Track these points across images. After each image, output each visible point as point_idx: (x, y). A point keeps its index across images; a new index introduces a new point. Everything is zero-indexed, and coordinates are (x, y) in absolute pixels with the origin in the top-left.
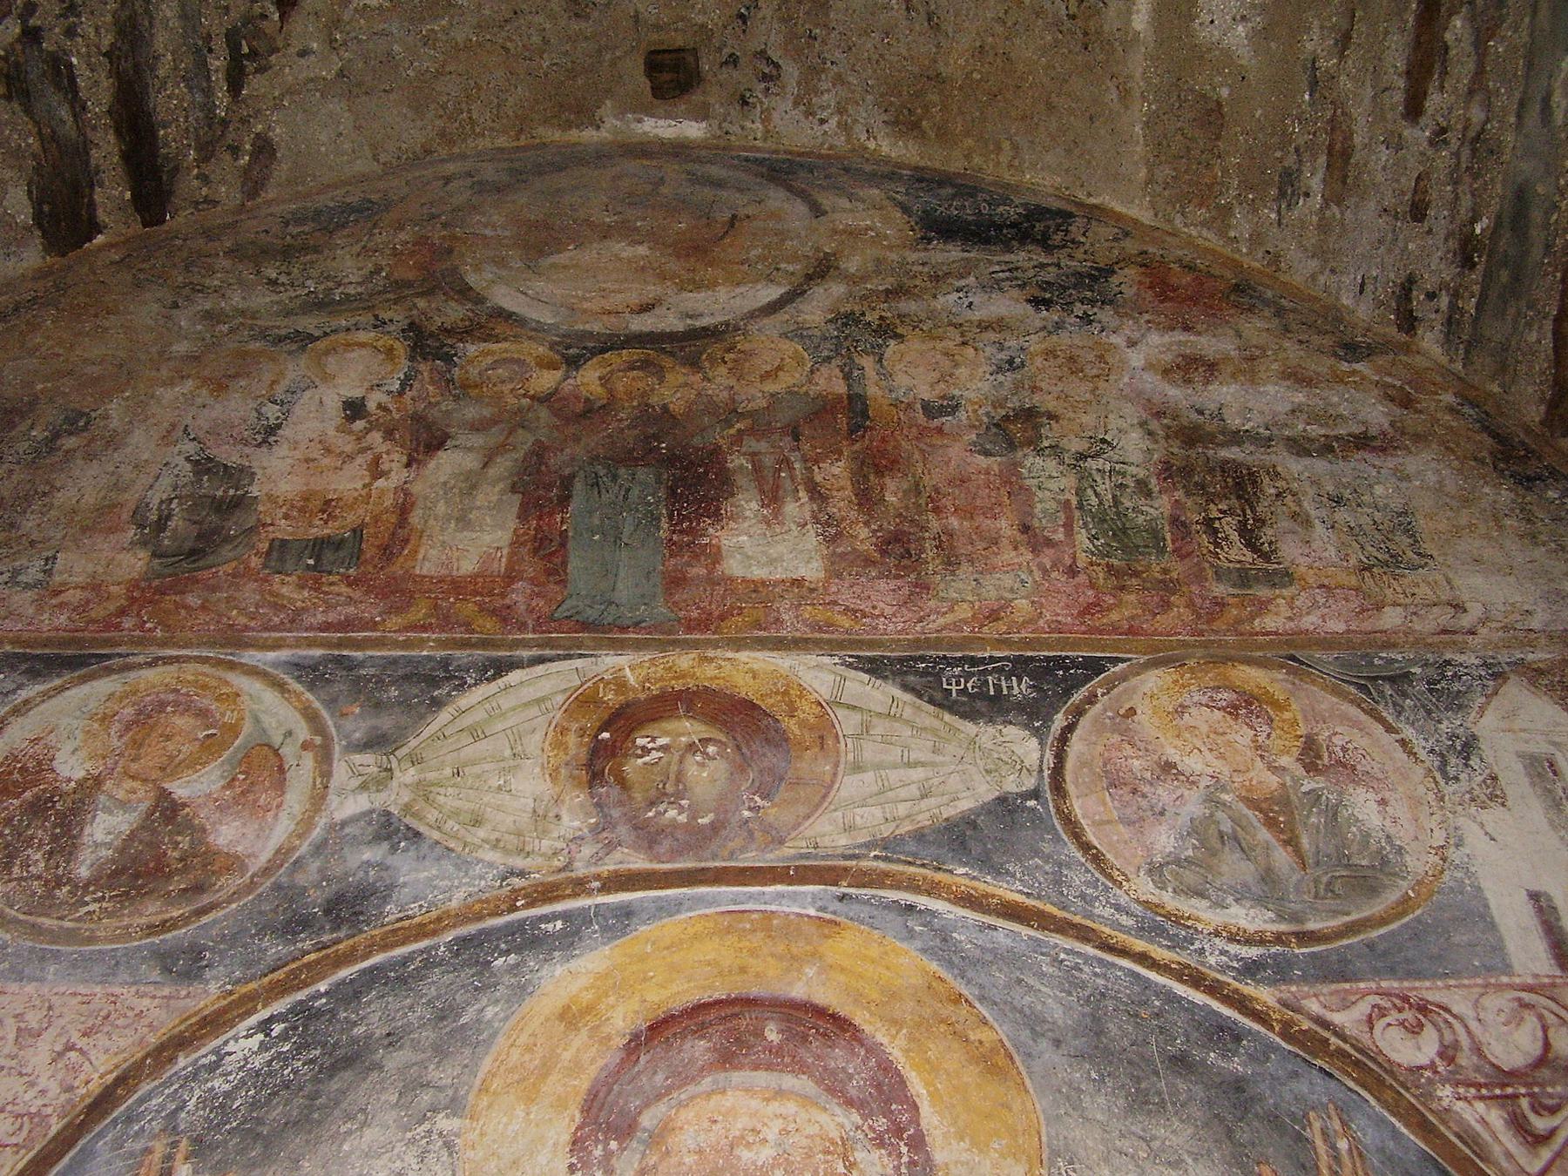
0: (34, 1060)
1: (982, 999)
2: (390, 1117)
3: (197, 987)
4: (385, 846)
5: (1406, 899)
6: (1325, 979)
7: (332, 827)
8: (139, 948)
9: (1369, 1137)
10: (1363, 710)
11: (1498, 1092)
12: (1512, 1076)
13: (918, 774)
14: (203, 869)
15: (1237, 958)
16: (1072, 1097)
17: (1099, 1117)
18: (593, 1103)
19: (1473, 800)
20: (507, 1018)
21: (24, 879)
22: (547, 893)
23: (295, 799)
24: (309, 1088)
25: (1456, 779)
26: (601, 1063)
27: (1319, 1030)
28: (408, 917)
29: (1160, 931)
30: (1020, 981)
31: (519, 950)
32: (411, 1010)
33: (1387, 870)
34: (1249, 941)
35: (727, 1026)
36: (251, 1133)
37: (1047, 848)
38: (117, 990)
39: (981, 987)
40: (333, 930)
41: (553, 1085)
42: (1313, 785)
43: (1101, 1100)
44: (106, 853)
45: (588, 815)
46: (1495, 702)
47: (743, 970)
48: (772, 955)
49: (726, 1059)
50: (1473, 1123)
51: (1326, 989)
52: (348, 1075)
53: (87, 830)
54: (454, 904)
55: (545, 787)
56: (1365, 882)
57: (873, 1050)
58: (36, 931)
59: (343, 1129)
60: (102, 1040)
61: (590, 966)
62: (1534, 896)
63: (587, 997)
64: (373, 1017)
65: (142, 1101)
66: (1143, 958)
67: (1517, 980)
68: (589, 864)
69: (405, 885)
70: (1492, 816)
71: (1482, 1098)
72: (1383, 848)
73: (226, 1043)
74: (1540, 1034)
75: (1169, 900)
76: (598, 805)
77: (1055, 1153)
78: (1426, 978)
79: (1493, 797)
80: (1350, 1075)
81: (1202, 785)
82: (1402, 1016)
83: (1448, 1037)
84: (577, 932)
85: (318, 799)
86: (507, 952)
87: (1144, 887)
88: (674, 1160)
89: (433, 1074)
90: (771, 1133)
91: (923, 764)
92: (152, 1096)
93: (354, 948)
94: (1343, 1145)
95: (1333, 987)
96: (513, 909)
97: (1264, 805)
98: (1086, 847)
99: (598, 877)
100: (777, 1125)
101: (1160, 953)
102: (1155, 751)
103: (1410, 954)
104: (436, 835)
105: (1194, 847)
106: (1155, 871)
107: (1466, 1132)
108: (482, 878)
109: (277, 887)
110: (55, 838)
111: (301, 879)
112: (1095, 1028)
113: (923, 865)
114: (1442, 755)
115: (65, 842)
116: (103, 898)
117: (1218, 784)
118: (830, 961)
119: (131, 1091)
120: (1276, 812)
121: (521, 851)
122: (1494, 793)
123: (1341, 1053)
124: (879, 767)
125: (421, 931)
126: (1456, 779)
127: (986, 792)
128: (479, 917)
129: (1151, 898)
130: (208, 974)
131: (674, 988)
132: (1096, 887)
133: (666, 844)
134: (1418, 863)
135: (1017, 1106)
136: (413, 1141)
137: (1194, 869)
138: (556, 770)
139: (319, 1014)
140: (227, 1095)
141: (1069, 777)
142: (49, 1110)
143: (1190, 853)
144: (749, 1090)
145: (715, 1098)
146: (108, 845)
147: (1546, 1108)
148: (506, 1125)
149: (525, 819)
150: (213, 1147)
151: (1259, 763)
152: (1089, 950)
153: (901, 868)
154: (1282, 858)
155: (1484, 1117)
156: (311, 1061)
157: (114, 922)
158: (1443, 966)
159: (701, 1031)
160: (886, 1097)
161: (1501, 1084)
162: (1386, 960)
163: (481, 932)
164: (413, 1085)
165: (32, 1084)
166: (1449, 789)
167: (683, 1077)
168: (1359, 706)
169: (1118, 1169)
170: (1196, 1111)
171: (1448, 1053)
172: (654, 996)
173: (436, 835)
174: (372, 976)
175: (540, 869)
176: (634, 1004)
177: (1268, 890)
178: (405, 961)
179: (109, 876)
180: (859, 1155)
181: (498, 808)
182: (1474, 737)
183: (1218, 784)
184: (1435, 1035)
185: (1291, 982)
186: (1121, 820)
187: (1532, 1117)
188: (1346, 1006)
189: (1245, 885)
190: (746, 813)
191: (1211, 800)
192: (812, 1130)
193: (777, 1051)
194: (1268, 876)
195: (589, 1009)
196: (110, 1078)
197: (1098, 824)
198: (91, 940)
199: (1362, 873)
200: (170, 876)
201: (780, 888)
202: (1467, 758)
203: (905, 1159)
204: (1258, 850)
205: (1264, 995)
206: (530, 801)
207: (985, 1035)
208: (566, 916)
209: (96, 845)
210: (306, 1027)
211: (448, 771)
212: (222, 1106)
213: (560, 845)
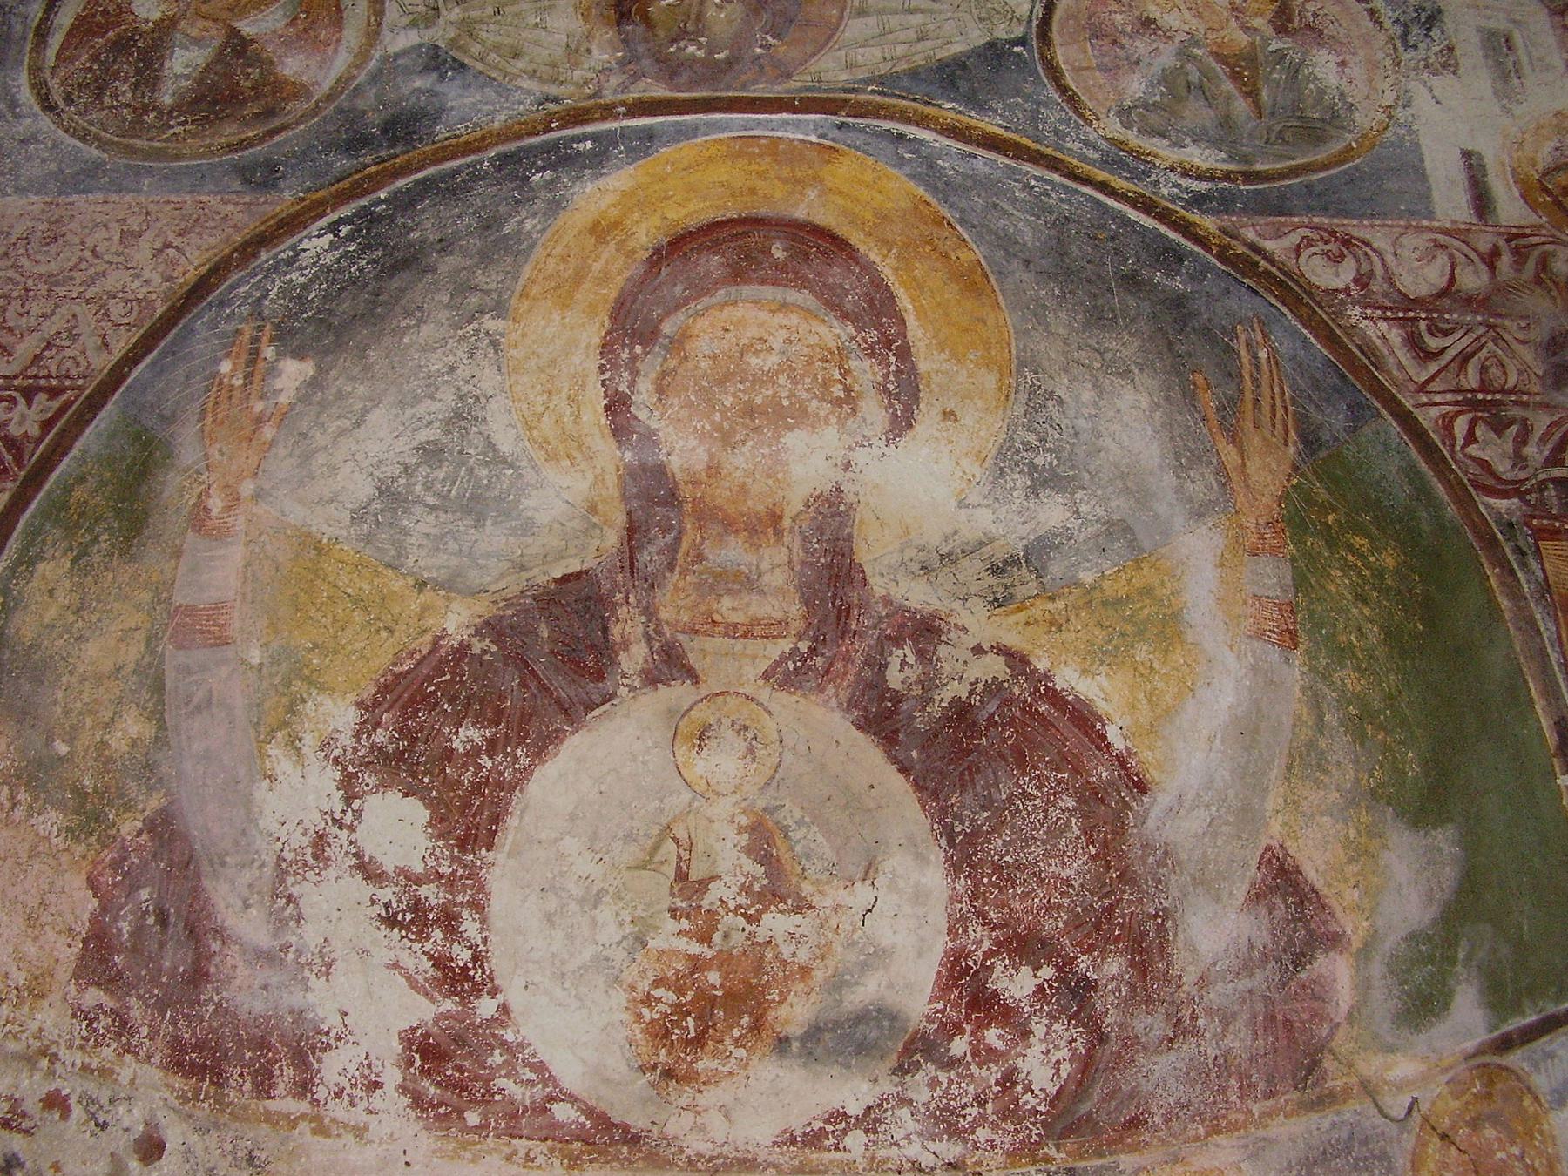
0: (138, 256)
1: (962, 221)
2: (443, 315)
3: (273, 195)
4: (435, 75)
5: (1349, 149)
7: (386, 59)
8: (221, 164)
9: (1285, 347)
12: (1417, 302)
13: (917, 19)
14: (274, 95)
15: (1187, 190)
16: (1039, 314)
17: (1061, 331)
18: (621, 311)
19: (1426, 66)
20: (544, 230)
21: (115, 107)
22: (578, 117)
23: (352, 35)
24: (373, 285)
25: (1415, 47)
26: (627, 274)
27: (1252, 254)
28: (456, 136)
29: (1122, 164)
30: (995, 206)
31: (554, 168)
32: (460, 219)
33: (1336, 123)
35: (737, 244)
36: (323, 322)
37: (1028, 88)
38: (203, 198)
39: (962, 211)
40: (389, 147)
41: (585, 294)
42: (1281, 45)
43: (1063, 315)
44: (185, 83)
45: (616, 50)
47: (753, 192)
48: (779, 178)
49: (737, 275)
52: (406, 275)
53: (167, 64)
54: (496, 125)
55: (577, 25)
56: (1313, 133)
57: (868, 267)
58: (131, 151)
59: (403, 324)
60: (195, 239)
61: (617, 184)
62: (1467, 154)
63: (616, 212)
64: (426, 224)
65: (233, 287)
66: (1103, 187)
67: (1437, 224)
68: (615, 92)
69: (452, 108)
70: (1443, 84)
72: (1335, 104)
73: (301, 241)
74: (1448, 270)
75: (1133, 138)
76: (624, 41)
77: (1022, 364)
78: (1354, 217)
79: (1445, 66)
80: (1272, 292)
81: (1177, 40)
82: (1328, 247)
83: (1365, 267)
84: (605, 152)
85: (373, 34)
86: (543, 169)
87: (1113, 126)
88: (690, 365)
89: (481, 279)
90: (777, 342)
91: (922, 11)
92: (241, 286)
93: (409, 162)
94: (1263, 354)
95: (1270, 219)
96: (549, 130)
97: (1232, 61)
98: (1063, 89)
99: (623, 103)
100: (783, 333)
101: (1119, 183)
102: (1137, 8)
103: (1344, 196)
104: (480, 66)
105: (1162, 94)
106: (1124, 113)
108: (520, 103)
109: (340, 110)
110: (138, 72)
111: (361, 104)
112: (1059, 249)
113: (915, 100)
114: (1405, 25)
115: (148, 75)
116: (186, 122)
118: (830, 185)
119: (222, 279)
120: (1244, 69)
121: (555, 80)
122: (1448, 62)
123: (1267, 272)
124: (881, 12)
125: (468, 149)
126: (1415, 47)
127: (978, 37)
128: (519, 137)
129: (1117, 136)
130: (282, 184)
131: (691, 207)
132: (1068, 125)
133: (684, 78)
134: (1365, 119)
135: (991, 322)
136: (463, 339)
137: (1155, 116)
138: (588, 9)
139: (380, 218)
140: (304, 287)
141: (1055, 26)
142: (154, 296)
143: (1158, 98)
144: (756, 303)
145: (727, 310)
146: (187, 77)
148: (544, 328)
149: (559, 53)
150: (292, 332)
151: (1233, 23)
152: (1056, 178)
153: (894, 101)
154: (1241, 107)
155: (1385, 335)
156: (375, 261)
157: (198, 142)
158: (1371, 209)
159: (715, 247)
160: (877, 313)
161: (1404, 309)
162: (1321, 199)
163: (521, 149)
164: (465, 288)
165: (138, 276)
166: (1406, 56)
167: (700, 289)
169: (1076, 379)
170: (1142, 325)
171: (1362, 280)
172: (673, 214)
173: (480, 66)
174: (426, 186)
175: (570, 95)
176: (656, 221)
177: (1224, 134)
178: (457, 171)
179: (190, 103)
180: (853, 364)
181: (536, 43)
182: (1440, 11)
184: (1353, 262)
185: (1234, 212)
186: (1101, 68)
187: (1428, 338)
188: (1279, 235)
189: (1204, 128)
190: (759, 50)
191: (1184, 54)
192: (812, 340)
193: (782, 268)
194: (1226, 122)
195: (617, 224)
196: (204, 269)
197: (1077, 70)
198: (178, 157)
199: (1312, 124)
200: (245, 101)
201: (785, 116)
202: (1428, 30)
203: (893, 368)
204: (1221, 100)
205: (1208, 223)
206: (564, 37)
207: (965, 256)
208: (594, 137)
209: (176, 76)
210: (369, 230)
211: (490, 10)
212: (300, 297)
213: (591, 75)
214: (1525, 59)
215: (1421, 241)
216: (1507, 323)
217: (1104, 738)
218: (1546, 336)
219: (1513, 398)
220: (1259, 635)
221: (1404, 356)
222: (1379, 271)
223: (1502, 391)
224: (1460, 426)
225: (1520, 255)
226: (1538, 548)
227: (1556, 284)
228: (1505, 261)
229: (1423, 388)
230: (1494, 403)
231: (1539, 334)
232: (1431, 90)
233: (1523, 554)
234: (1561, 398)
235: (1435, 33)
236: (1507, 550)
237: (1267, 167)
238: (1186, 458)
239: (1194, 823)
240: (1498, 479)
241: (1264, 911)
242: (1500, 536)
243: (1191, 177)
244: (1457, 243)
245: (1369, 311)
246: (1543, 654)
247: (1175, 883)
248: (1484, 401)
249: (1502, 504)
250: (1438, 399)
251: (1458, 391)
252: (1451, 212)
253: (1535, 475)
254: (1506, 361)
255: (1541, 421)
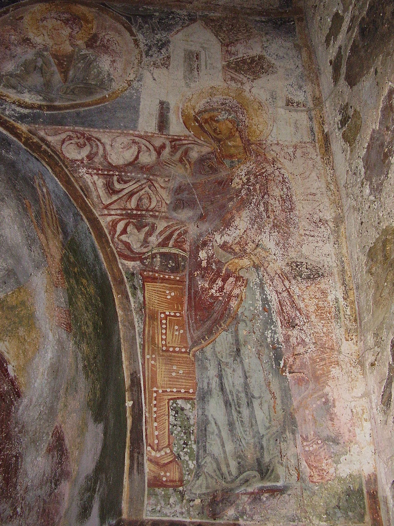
6: (52, 124)
10: (125, 27)
11: (106, 173)
12: (116, 168)
27: (40, 142)
34: (26, 107)
42: (87, 52)
46: (185, 29)
50: (89, 183)
51: (49, 127)
62: (162, 103)
67: (137, 133)
71: (97, 174)
72: (104, 78)
78: (96, 128)
80: (45, 160)
81: (38, 48)
103: (94, 118)
105: (21, 70)
107: (85, 186)
117: (46, 48)
122: (166, 63)
123: (45, 152)
143: (19, 72)
147: (123, 180)
151: (67, 42)
154: (58, 77)
158: (106, 125)
166: (145, 59)
168: (123, 25)
171: (90, 157)
177: (46, 89)
182: (169, 42)
183: (46, 48)
187: (116, 184)
188: (56, 134)
189: (36, 86)
191: (39, 54)
194: (48, 85)
202: (161, 49)
205: (23, 127)
214: (203, 63)
215: (126, 140)
216: (159, 179)
217: (7, 370)
218: (176, 185)
219: (151, 213)
220: (60, 325)
221: (102, 192)
222: (101, 152)
223: (147, 210)
224: (120, 227)
225: (175, 149)
226: (143, 285)
227: (190, 163)
228: (167, 151)
229: (107, 207)
230: (141, 216)
231: (173, 185)
232: (152, 74)
233: (135, 288)
234: (176, 215)
235: (163, 51)
236: (128, 286)
237: (59, 104)
238: (31, 241)
239: (34, 413)
240: (132, 251)
241: (50, 457)
242: (125, 279)
243: (22, 107)
244: (144, 141)
245: (90, 171)
246: (134, 338)
247: (25, 440)
248: (136, 215)
249: (130, 264)
250: (113, 212)
251: (124, 209)
252: (146, 128)
253: (151, 251)
254: (153, 196)
255: (161, 225)
